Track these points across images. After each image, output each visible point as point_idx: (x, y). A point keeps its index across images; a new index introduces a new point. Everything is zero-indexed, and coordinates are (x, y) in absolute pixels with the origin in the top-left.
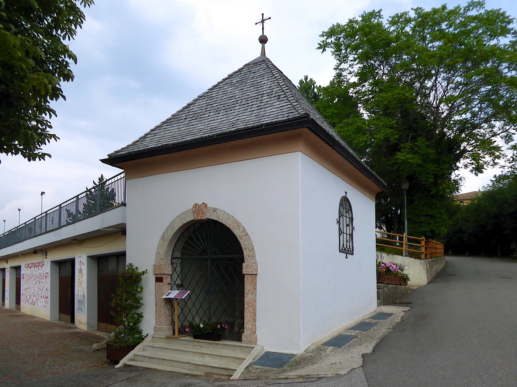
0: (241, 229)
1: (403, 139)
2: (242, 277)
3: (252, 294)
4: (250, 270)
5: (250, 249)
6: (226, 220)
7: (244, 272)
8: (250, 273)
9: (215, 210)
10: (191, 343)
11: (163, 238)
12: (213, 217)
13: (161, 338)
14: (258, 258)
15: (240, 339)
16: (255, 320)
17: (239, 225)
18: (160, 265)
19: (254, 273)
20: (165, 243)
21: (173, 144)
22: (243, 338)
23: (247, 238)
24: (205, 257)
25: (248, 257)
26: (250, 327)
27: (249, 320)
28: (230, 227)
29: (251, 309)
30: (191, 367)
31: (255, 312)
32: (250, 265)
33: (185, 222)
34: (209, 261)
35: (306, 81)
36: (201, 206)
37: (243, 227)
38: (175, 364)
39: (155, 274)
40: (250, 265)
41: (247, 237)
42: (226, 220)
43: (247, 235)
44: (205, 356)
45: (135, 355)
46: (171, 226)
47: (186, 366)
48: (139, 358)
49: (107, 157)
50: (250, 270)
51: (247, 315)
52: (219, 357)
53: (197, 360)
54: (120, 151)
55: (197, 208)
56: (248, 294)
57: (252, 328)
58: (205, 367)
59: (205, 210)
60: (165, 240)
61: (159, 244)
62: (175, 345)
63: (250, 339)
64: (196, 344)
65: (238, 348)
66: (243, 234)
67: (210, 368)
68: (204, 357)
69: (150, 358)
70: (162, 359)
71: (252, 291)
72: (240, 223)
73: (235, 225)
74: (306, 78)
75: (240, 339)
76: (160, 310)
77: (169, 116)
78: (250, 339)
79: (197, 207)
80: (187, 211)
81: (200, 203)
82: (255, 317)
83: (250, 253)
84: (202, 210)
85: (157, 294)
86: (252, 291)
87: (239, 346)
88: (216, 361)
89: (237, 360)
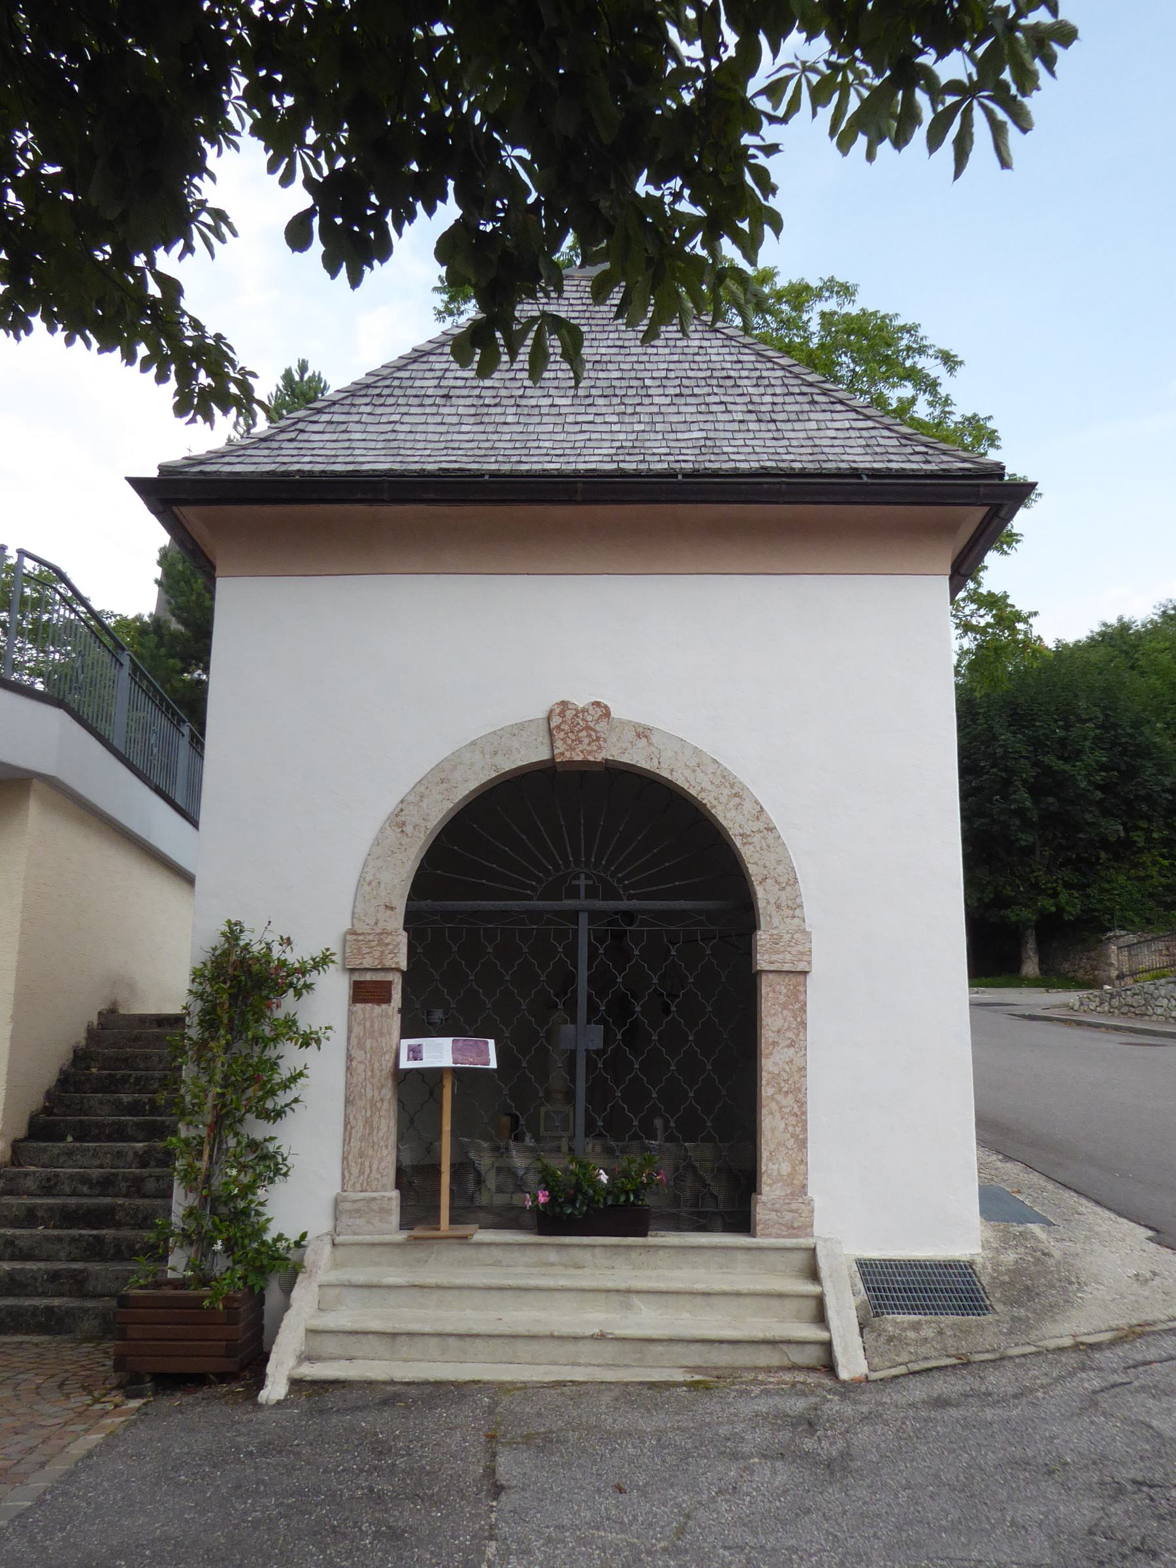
0: (748, 805)
1: (40, 618)
2: (746, 985)
3: (791, 1045)
4: (788, 957)
5: (783, 879)
6: (687, 772)
7: (763, 960)
8: (787, 967)
9: (643, 733)
10: (531, 1256)
11: (397, 820)
12: (637, 756)
13: (373, 1245)
14: (813, 914)
15: (742, 1222)
16: (802, 1144)
17: (739, 794)
18: (385, 932)
19: (801, 966)
20: (405, 841)
21: (494, 474)
22: (761, 1213)
23: (771, 840)
24: (569, 904)
25: (772, 909)
26: (786, 1168)
27: (779, 1144)
28: (707, 799)
29: (789, 1101)
30: (608, 1351)
31: (804, 1113)
32: (787, 937)
33: (508, 764)
34: (583, 918)
35: (302, 377)
36: (584, 710)
37: (757, 802)
38: (524, 1349)
39: (352, 970)
40: (787, 937)
41: (770, 836)
42: (687, 772)
43: (771, 829)
44: (635, 1299)
45: (312, 1332)
46: (440, 774)
47: (585, 1350)
48: (329, 1345)
49: (154, 473)
50: (788, 957)
51: (772, 1125)
52: (699, 1300)
53: (648, 1320)
54: (199, 461)
55: (561, 720)
56: (775, 1043)
57: (791, 1175)
58: (678, 1348)
59: (602, 726)
60: (409, 829)
61: (377, 842)
62: (443, 1266)
63: (788, 1216)
64: (552, 1256)
65: (740, 1256)
66: (757, 825)
67: (698, 1347)
68: (628, 1307)
69: (394, 1335)
70: (460, 1336)
71: (790, 1034)
72: (744, 788)
73: (726, 791)
74: (303, 367)
75: (742, 1222)
76: (368, 1122)
77: (359, 375)
78: (788, 1216)
79: (569, 714)
80: (522, 726)
81: (581, 701)
82: (805, 1130)
83: (783, 895)
84: (588, 728)
85: (358, 1054)
86: (790, 1034)
87: (749, 1249)
88: (686, 1315)
89: (775, 1303)
